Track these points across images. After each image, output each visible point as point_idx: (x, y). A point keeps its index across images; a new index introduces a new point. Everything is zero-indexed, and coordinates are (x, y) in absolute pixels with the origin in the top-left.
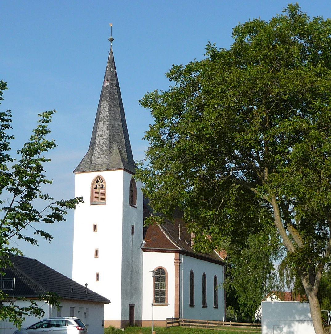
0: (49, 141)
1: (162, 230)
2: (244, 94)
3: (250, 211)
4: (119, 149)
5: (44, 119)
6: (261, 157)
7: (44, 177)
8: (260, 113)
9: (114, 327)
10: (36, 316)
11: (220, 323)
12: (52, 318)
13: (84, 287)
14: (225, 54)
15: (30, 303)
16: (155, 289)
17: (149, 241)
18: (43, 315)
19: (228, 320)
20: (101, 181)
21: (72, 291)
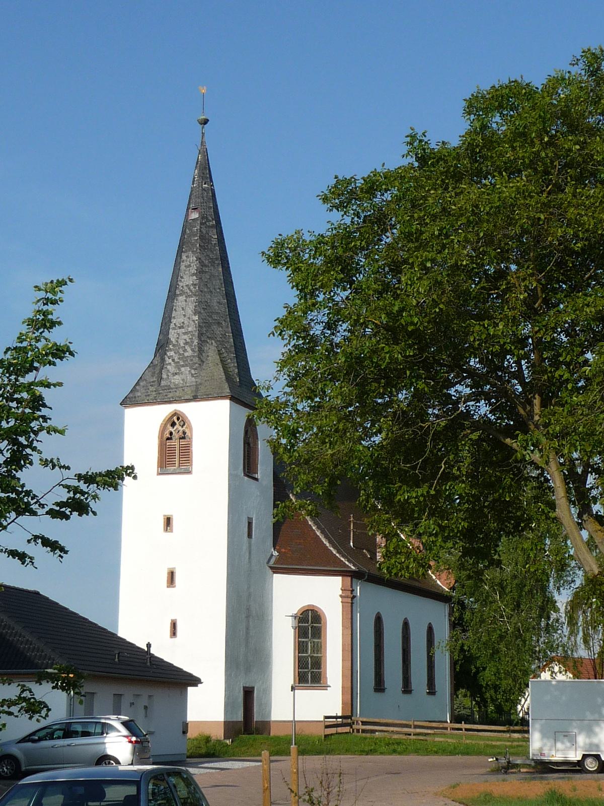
0: (58, 344)
1: (314, 528)
2: (489, 240)
3: (504, 489)
4: (220, 354)
5: (48, 297)
6: (526, 372)
7: (48, 420)
8: (524, 280)
9: (210, 737)
10: (30, 718)
11: (441, 726)
12: (73, 719)
13: (143, 650)
14: (447, 154)
15: (19, 690)
16: (299, 653)
17: (287, 551)
18: (47, 715)
19: (456, 719)
20: (182, 423)
21: (117, 660)
